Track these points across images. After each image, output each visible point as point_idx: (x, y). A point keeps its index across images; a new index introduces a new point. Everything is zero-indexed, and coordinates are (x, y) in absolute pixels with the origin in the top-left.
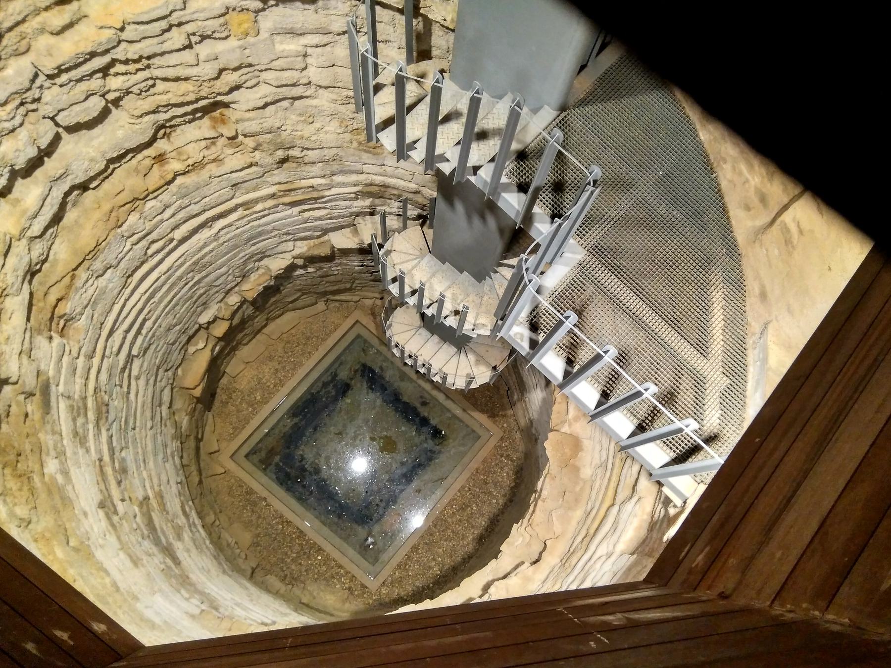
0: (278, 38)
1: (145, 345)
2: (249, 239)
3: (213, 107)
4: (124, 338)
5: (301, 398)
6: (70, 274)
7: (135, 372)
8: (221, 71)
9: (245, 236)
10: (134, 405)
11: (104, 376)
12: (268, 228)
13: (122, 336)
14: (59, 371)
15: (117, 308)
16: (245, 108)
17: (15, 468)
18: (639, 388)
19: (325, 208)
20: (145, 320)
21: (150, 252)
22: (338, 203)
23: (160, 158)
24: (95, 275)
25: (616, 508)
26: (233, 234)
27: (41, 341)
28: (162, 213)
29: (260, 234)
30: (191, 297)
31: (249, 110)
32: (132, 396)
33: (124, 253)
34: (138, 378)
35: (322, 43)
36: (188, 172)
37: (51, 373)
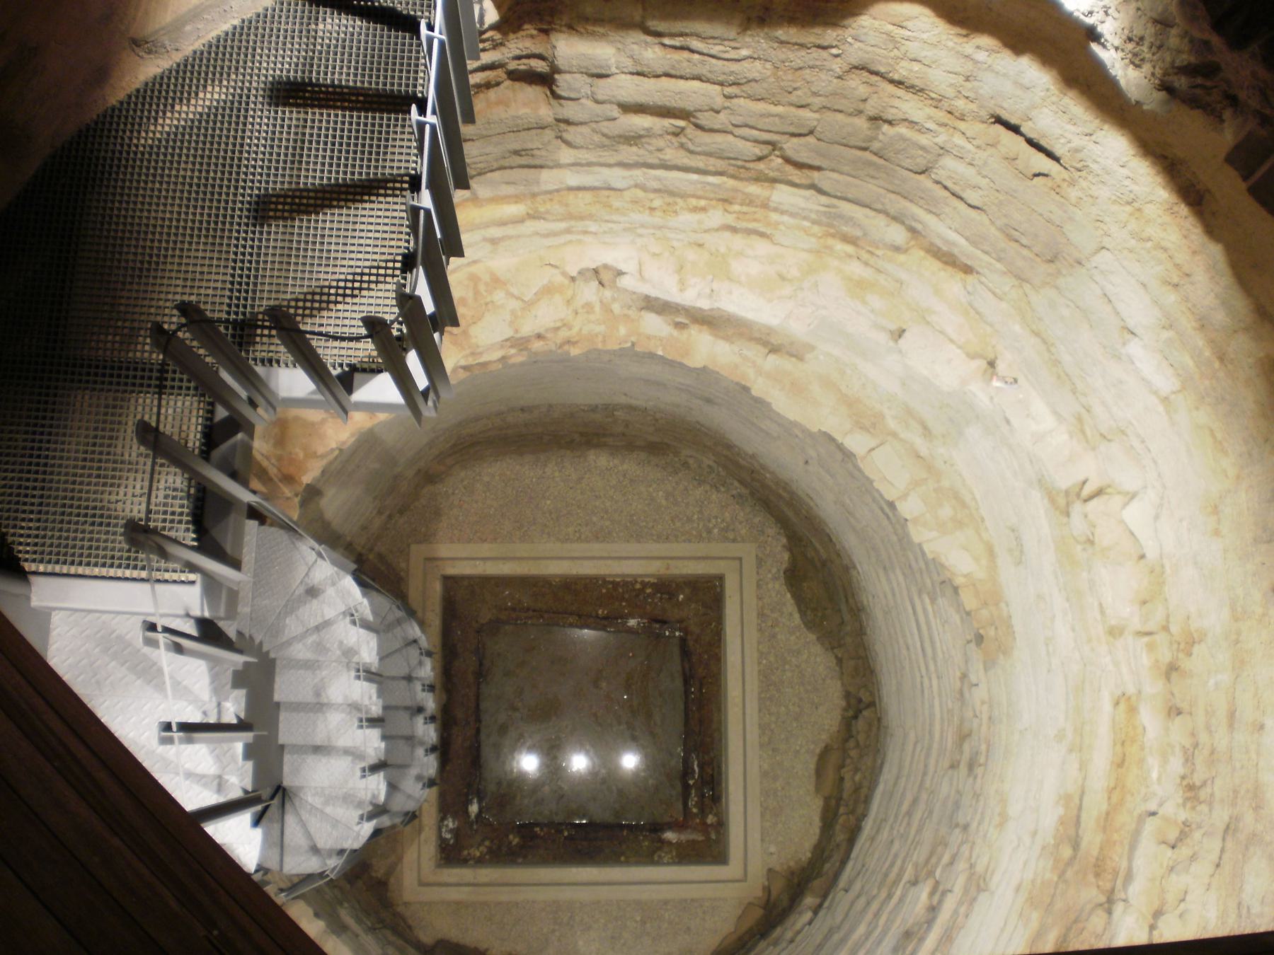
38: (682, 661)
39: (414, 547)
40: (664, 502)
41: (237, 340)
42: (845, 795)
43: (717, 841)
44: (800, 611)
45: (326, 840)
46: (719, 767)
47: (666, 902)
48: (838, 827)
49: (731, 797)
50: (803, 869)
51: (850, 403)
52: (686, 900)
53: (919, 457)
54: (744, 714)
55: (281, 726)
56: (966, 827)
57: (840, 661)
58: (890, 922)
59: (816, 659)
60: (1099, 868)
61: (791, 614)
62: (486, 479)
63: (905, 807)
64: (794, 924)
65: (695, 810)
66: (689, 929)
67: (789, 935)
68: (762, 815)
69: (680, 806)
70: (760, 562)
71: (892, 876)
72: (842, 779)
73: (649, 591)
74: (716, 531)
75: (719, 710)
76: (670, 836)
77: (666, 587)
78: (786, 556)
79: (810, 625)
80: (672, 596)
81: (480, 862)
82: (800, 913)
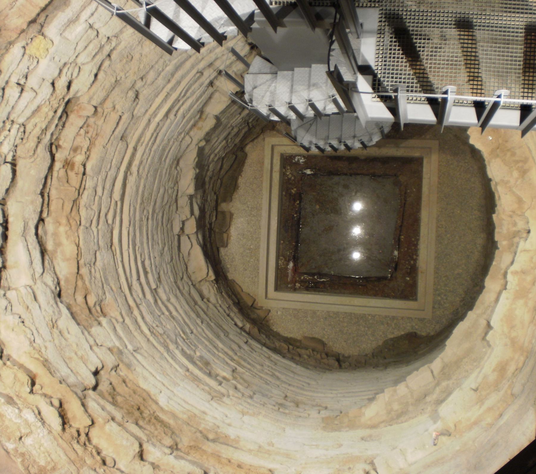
0: (66, 34)
1: (156, 276)
2: (160, 158)
3: (68, 107)
4: (141, 284)
6: (78, 277)
7: (164, 298)
8: (53, 84)
9: (156, 160)
10: (180, 318)
11: (148, 318)
12: (165, 142)
13: (138, 285)
14: (120, 338)
15: (121, 270)
16: (86, 89)
17: (144, 418)
18: (495, 99)
19: (188, 98)
20: (143, 263)
21: (110, 222)
22: (193, 88)
23: (68, 164)
24: (92, 265)
26: (147, 165)
27: (95, 330)
28: (96, 194)
29: (164, 150)
30: (158, 224)
31: (89, 88)
32: (174, 313)
33: (96, 236)
34: (169, 300)
35: (94, 10)
36: (89, 156)
37: (117, 344)
38: (376, 277)
39: (437, 142)
40: (456, 272)
41: (392, 16)
42: (298, 350)
43: (287, 287)
44: (394, 338)
45: (257, 93)
46: (322, 291)
47: (258, 260)
48: (283, 344)
49: (306, 296)
50: (268, 326)
51: (457, 363)
52: (258, 270)
53: (425, 396)
54: (345, 305)
55: (303, 69)
56: (251, 397)
57: (366, 355)
58: (218, 358)
59: (369, 344)
60: (195, 448)
61: (393, 333)
62: (472, 180)
63: (277, 374)
64: (237, 317)
65: (302, 278)
66: (246, 270)
67: (232, 314)
68: (295, 310)
69: (305, 271)
70: (422, 320)
71: (243, 363)
72: (307, 349)
73: (412, 262)
74: (439, 298)
75: (351, 294)
76: (291, 265)
77: (413, 271)
78: (424, 334)
79: (386, 342)
81: (283, 174)
82: (242, 321)
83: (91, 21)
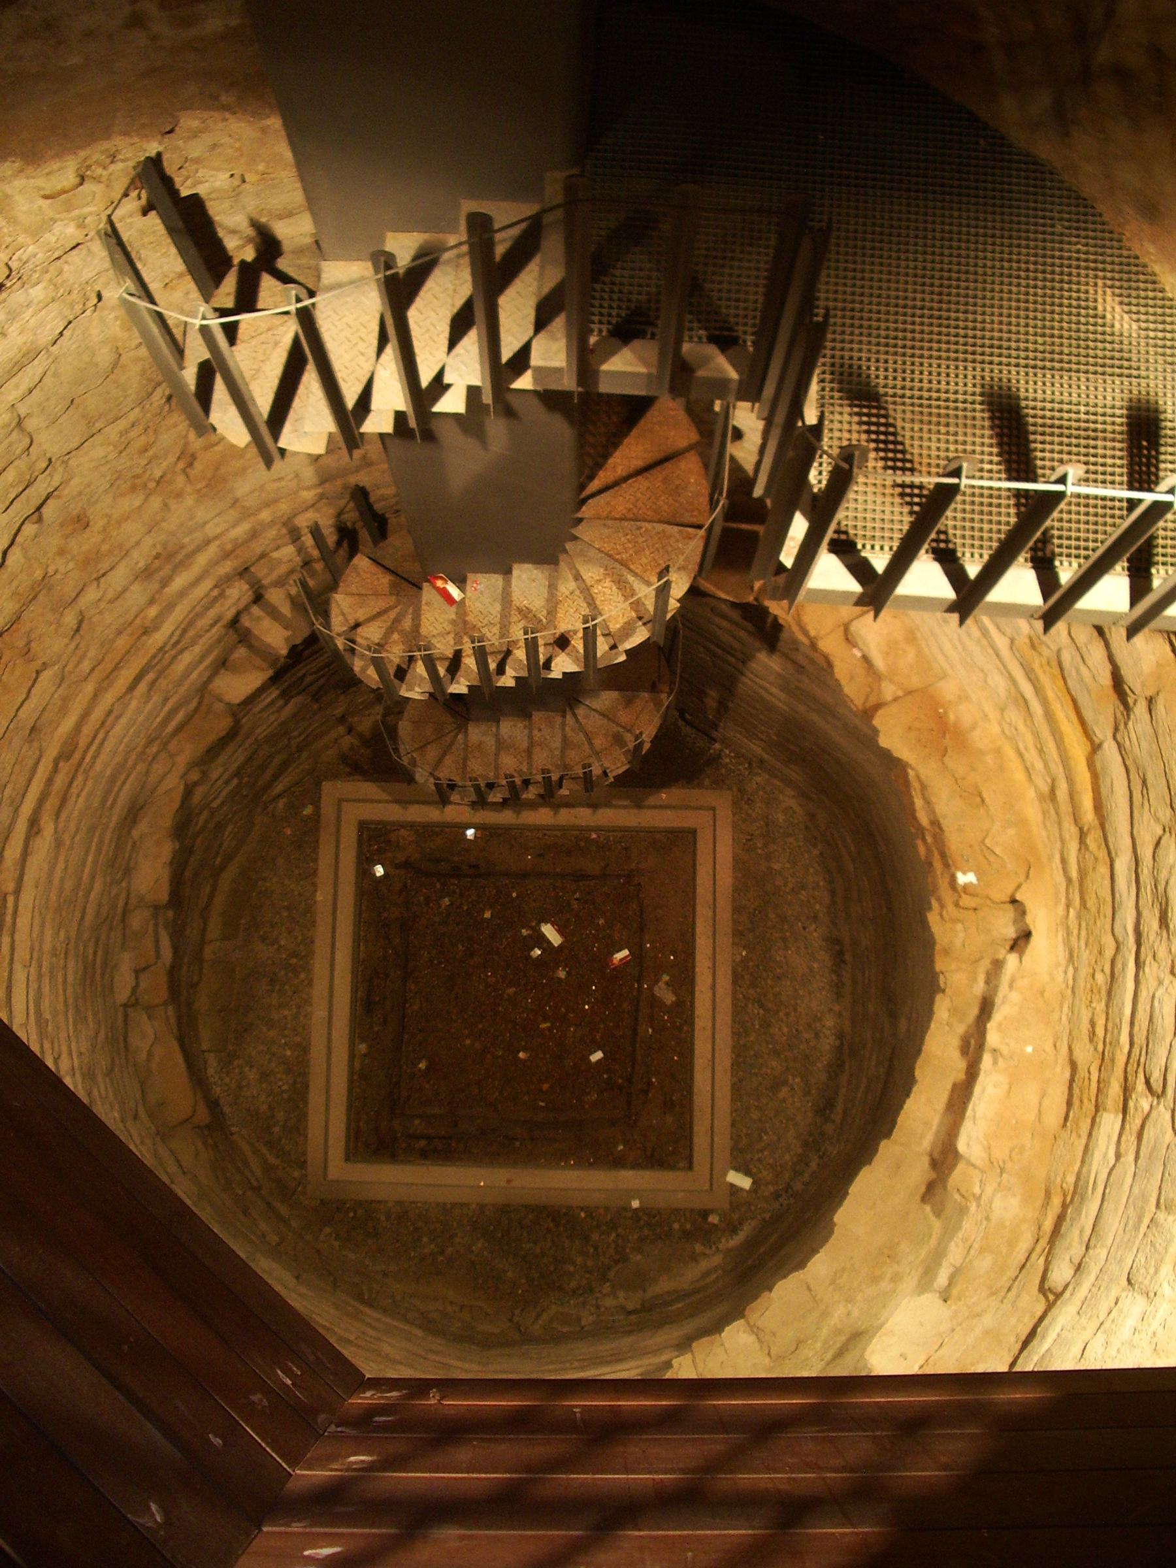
5: (354, 1000)
9: (96, 802)
25: (1109, 748)
80: (668, 1105)
83: (22, 410)
